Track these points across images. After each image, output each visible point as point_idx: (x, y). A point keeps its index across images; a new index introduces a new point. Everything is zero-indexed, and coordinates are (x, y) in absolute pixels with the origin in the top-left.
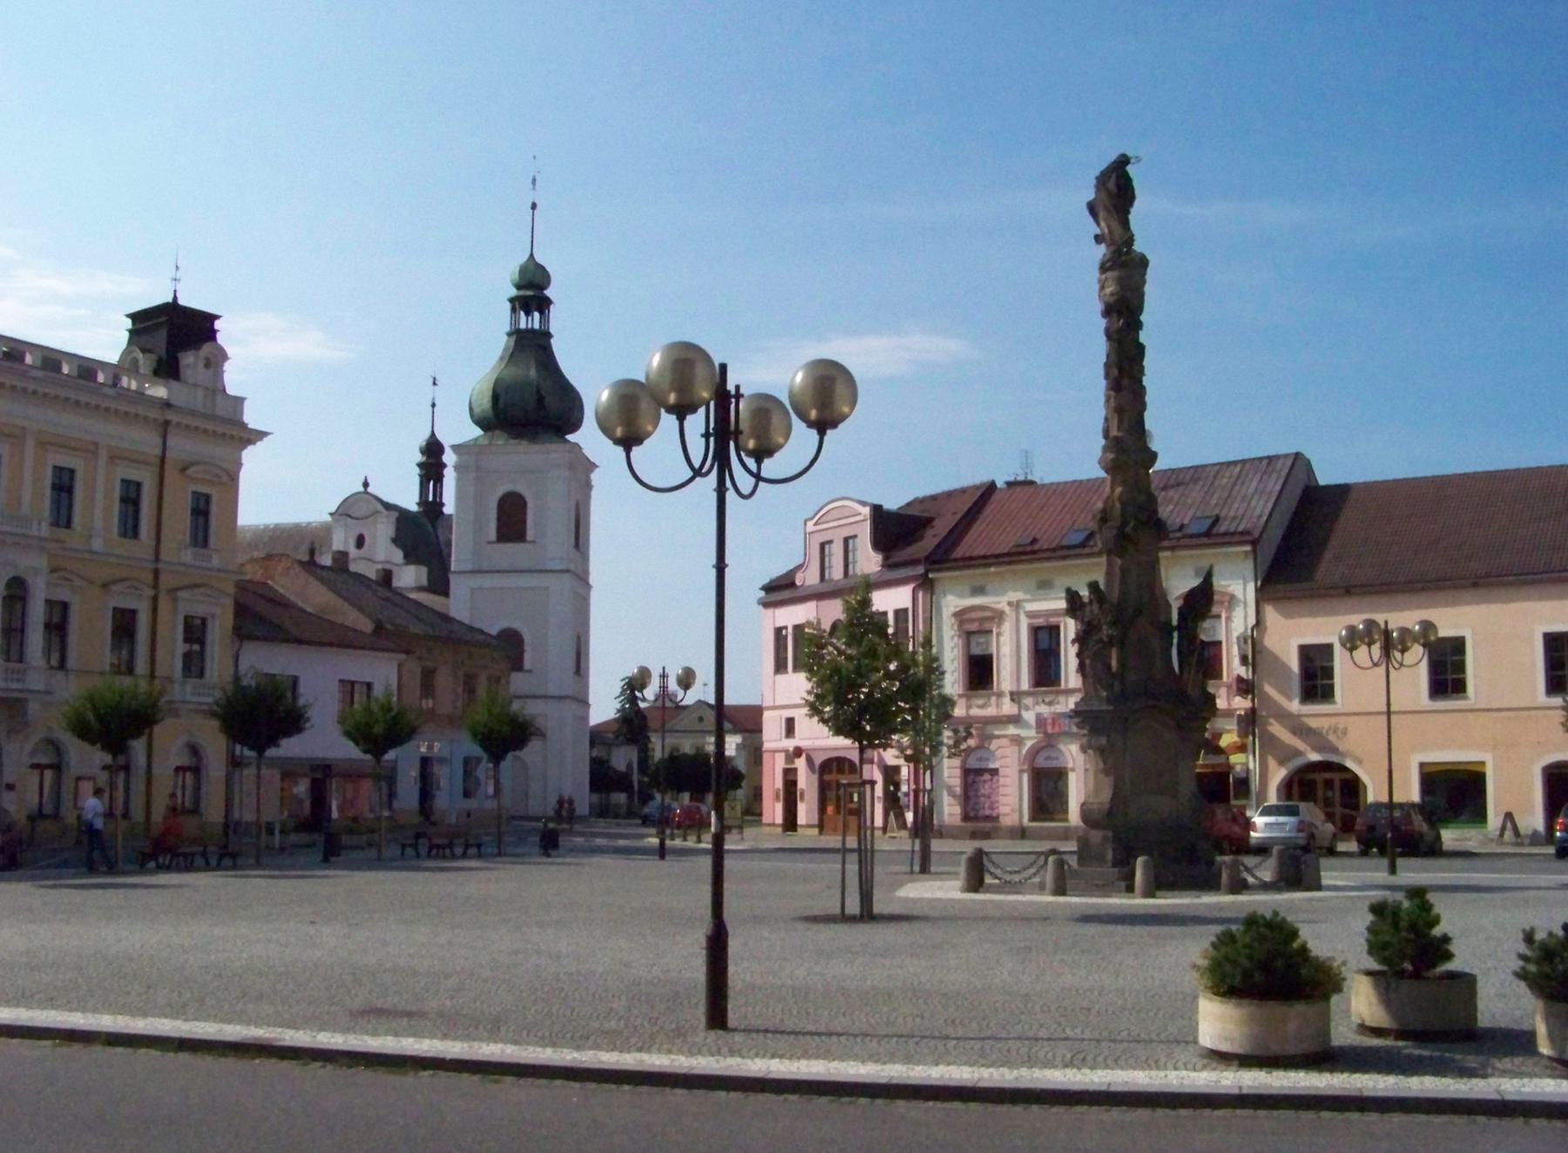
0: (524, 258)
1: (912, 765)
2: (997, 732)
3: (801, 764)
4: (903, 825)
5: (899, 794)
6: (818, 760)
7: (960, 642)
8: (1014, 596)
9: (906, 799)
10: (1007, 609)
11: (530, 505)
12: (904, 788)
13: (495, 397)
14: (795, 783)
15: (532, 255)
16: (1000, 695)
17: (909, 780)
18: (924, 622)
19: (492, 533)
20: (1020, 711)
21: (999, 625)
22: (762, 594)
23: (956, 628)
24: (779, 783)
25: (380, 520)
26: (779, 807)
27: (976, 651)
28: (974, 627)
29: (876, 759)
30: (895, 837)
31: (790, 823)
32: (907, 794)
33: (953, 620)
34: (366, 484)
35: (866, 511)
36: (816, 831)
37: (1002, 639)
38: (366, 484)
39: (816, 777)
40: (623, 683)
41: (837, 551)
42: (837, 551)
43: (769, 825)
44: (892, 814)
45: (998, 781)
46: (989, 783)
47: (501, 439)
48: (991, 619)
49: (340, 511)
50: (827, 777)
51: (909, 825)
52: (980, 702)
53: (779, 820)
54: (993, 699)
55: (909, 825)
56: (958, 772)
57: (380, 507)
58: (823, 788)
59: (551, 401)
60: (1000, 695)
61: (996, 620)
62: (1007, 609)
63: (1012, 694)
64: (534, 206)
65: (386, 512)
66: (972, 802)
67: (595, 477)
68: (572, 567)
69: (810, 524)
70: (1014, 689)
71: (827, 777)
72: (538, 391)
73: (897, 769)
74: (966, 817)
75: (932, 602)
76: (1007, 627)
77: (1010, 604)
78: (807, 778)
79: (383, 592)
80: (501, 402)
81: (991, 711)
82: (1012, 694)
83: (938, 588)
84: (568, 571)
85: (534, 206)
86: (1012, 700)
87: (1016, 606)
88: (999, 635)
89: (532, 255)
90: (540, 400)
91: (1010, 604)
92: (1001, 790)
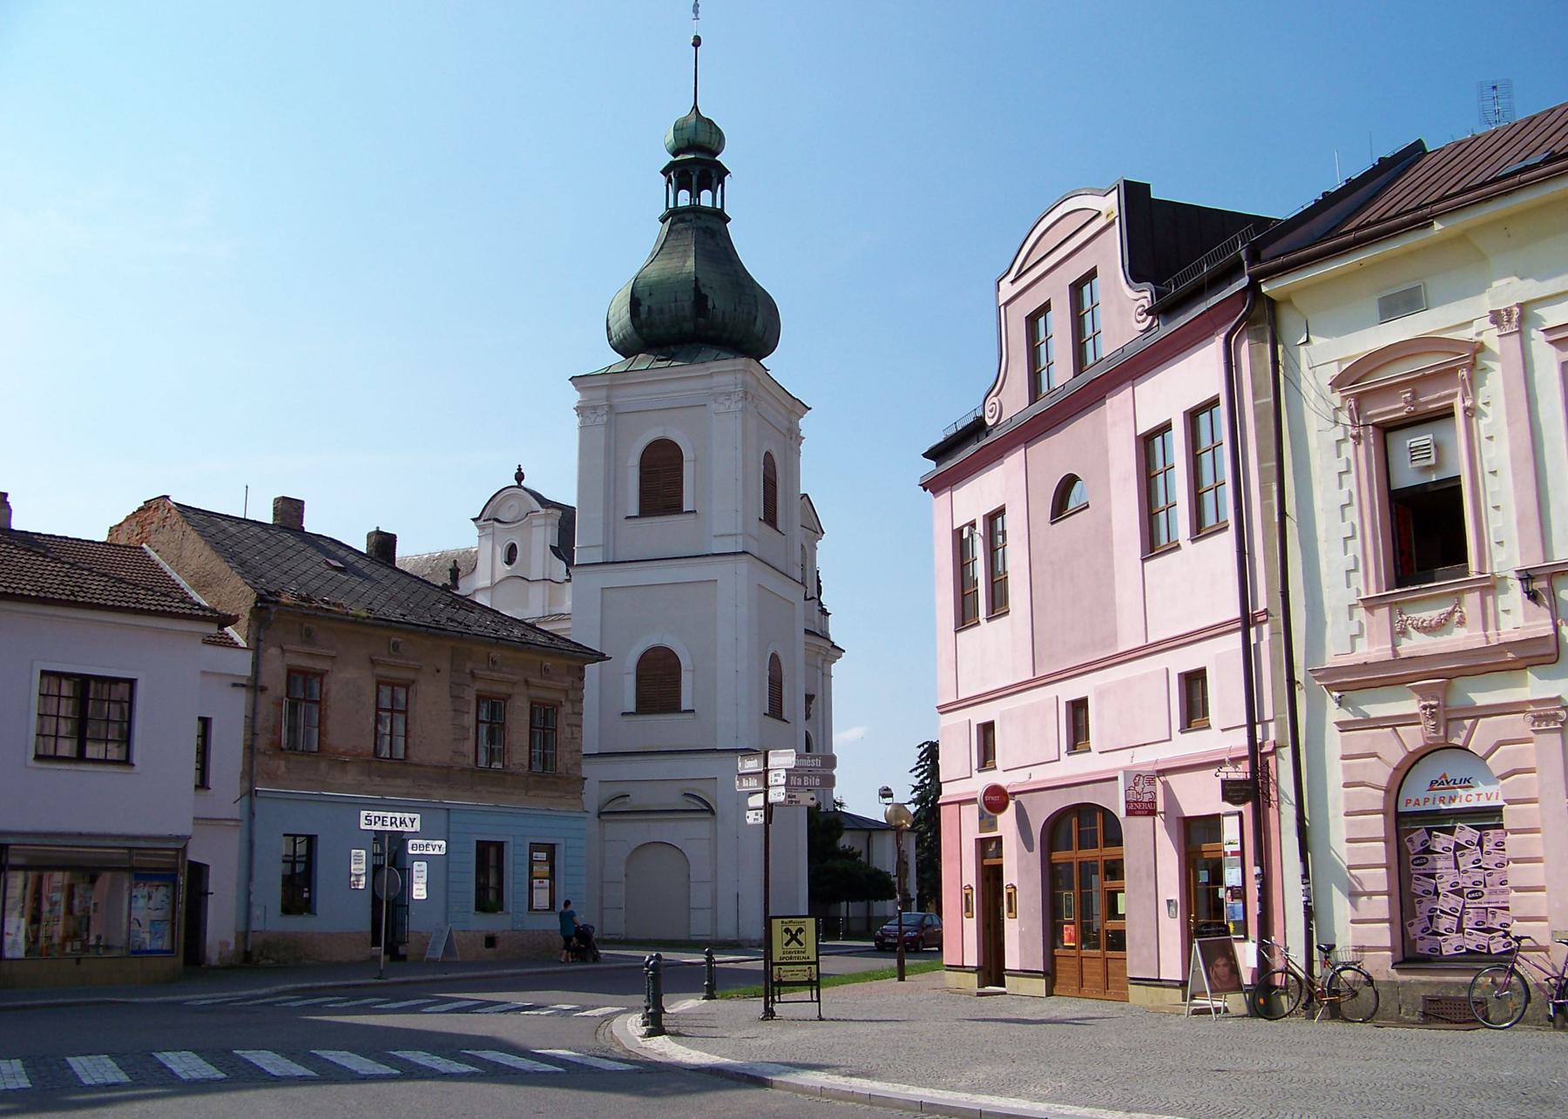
0: (685, 110)
1: (1247, 809)
2: (1481, 699)
3: (1006, 823)
4: (1229, 979)
5: (1221, 893)
6: (1040, 812)
7: (1358, 456)
8: (1508, 291)
9: (1239, 904)
10: (1491, 337)
11: (687, 455)
12: (1232, 876)
13: (635, 303)
14: (998, 870)
15: (695, 107)
16: (1490, 586)
17: (1242, 853)
18: (1257, 419)
19: (631, 501)
20: (1556, 628)
21: (1472, 386)
22: (931, 465)
23: (1344, 418)
24: (970, 877)
25: (535, 522)
26: (971, 926)
27: (1407, 476)
28: (1397, 407)
29: (1160, 807)
30: (1207, 1011)
31: (992, 969)
32: (1239, 893)
33: (1336, 399)
34: (520, 476)
35: (1110, 204)
36: (1040, 985)
37: (1482, 426)
38: (520, 476)
39: (1036, 855)
40: (922, 749)
41: (1059, 325)
42: (1059, 325)
43: (951, 968)
44: (1196, 945)
45: (1500, 845)
46: (1473, 853)
47: (643, 361)
48: (1445, 374)
49: (485, 516)
50: (1059, 856)
51: (1247, 979)
52: (1431, 615)
53: (972, 959)
54: (1471, 601)
55: (1247, 979)
56: (1377, 825)
57: (536, 505)
58: (1053, 878)
59: (718, 302)
60: (1490, 586)
61: (1463, 373)
62: (1491, 337)
63: (1527, 577)
64: (697, 42)
65: (543, 511)
66: (1422, 910)
67: (805, 424)
68: (753, 549)
69: (1005, 284)
70: (1535, 561)
71: (1059, 856)
72: (697, 289)
73: (1212, 824)
74: (1408, 957)
75: (1275, 362)
76: (1496, 387)
77: (1496, 318)
78: (1020, 859)
79: (380, 572)
80: (643, 309)
81: (1463, 638)
82: (1527, 577)
83: (1289, 321)
84: (744, 553)
85: (697, 42)
86: (1533, 596)
87: (1518, 319)
88: (1470, 412)
89: (695, 107)
90: (700, 300)
91: (1496, 318)
92: (1517, 874)
